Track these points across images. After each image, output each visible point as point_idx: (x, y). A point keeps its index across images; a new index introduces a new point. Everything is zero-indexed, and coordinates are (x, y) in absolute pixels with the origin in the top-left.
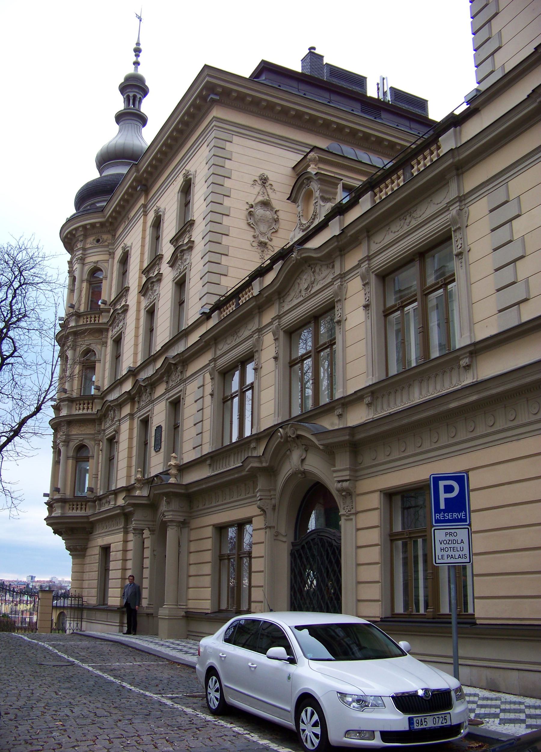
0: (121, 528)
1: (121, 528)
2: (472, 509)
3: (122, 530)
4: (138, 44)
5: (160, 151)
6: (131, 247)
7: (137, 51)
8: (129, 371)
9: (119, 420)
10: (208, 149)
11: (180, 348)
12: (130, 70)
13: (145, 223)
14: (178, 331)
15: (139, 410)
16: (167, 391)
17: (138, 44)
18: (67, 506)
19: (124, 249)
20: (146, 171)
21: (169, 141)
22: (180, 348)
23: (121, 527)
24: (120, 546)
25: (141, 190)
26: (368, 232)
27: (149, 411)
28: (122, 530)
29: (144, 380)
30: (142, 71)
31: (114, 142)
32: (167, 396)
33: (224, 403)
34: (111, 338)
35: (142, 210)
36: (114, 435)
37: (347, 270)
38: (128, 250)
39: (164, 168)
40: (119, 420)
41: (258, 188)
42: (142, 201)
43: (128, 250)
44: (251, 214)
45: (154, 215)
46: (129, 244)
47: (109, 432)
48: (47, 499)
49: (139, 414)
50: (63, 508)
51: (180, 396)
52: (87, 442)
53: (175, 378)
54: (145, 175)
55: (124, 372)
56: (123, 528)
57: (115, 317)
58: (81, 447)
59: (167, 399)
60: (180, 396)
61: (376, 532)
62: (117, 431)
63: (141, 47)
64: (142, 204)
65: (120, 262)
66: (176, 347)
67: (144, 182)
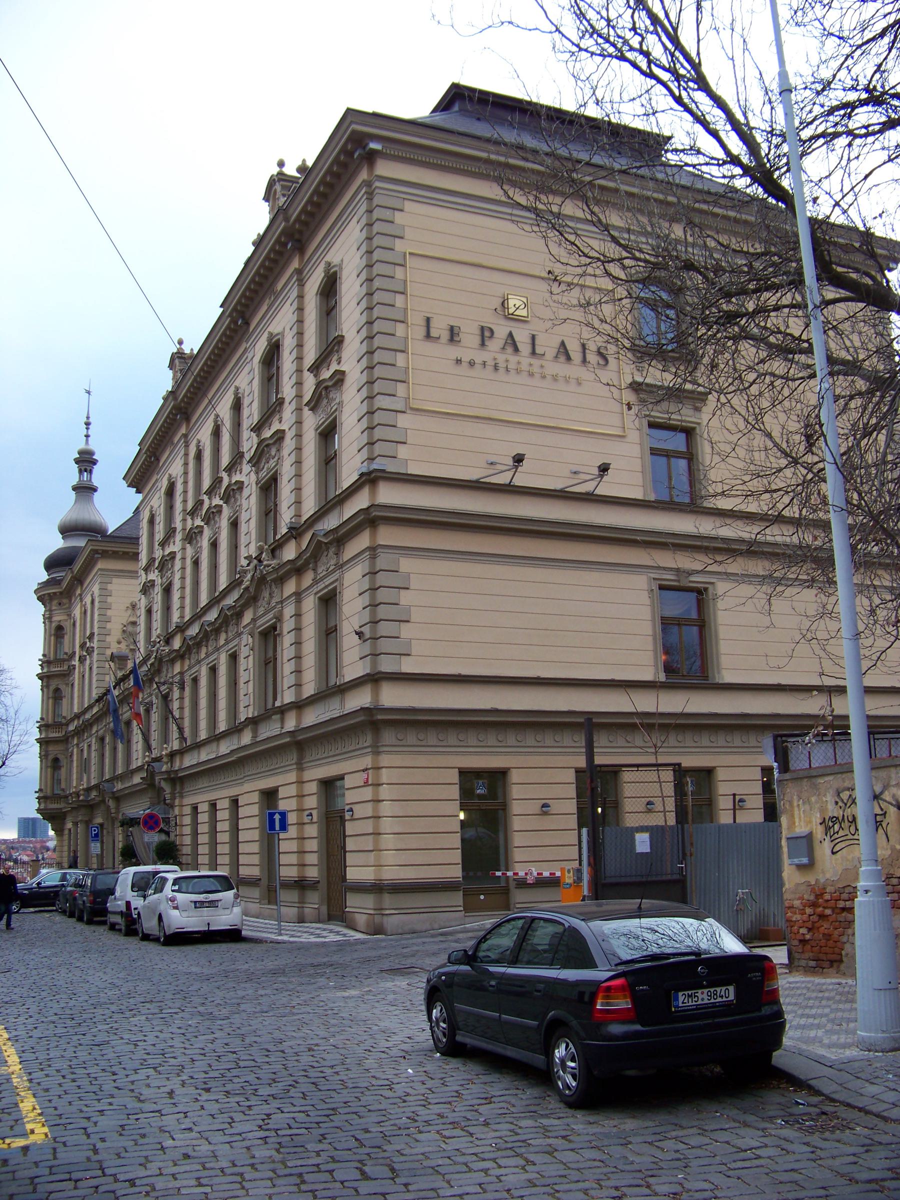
0: (368, 747)
1: (368, 747)
2: (893, 742)
3: (295, 767)
4: (88, 418)
5: (329, 172)
6: (340, 266)
7: (88, 424)
8: (177, 627)
9: (282, 602)
10: (359, 227)
11: (331, 522)
12: (82, 446)
13: (186, 455)
14: (326, 498)
15: (190, 668)
16: (316, 582)
17: (88, 418)
18: (48, 801)
19: (169, 480)
20: (182, 400)
21: (328, 179)
22: (331, 522)
23: (294, 762)
24: (292, 790)
25: (294, 248)
26: (315, 558)
27: (337, 580)
28: (369, 750)
29: (326, 534)
30: (92, 446)
31: (69, 518)
32: (315, 589)
33: (327, 635)
34: (257, 484)
35: (295, 279)
36: (275, 623)
37: (303, 588)
38: (279, 340)
39: (344, 187)
40: (282, 602)
41: (129, 612)
42: (295, 264)
43: (279, 340)
44: (124, 631)
45: (323, 275)
46: (336, 261)
47: (265, 621)
48: (37, 795)
49: (189, 673)
50: (45, 802)
51: (335, 588)
52: (59, 756)
53: (328, 561)
54: (297, 226)
55: (284, 530)
56: (296, 764)
57: (263, 449)
58: (56, 760)
59: (316, 594)
60: (335, 588)
61: (257, 832)
62: (279, 618)
63: (91, 420)
64: (295, 269)
65: (321, 294)
66: (326, 520)
67: (297, 236)
